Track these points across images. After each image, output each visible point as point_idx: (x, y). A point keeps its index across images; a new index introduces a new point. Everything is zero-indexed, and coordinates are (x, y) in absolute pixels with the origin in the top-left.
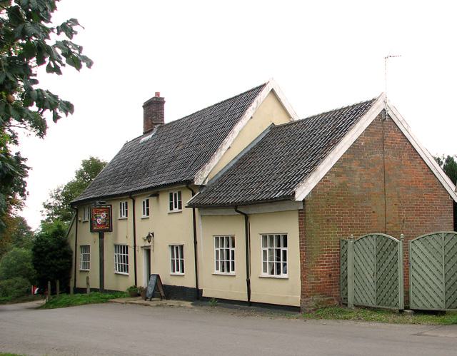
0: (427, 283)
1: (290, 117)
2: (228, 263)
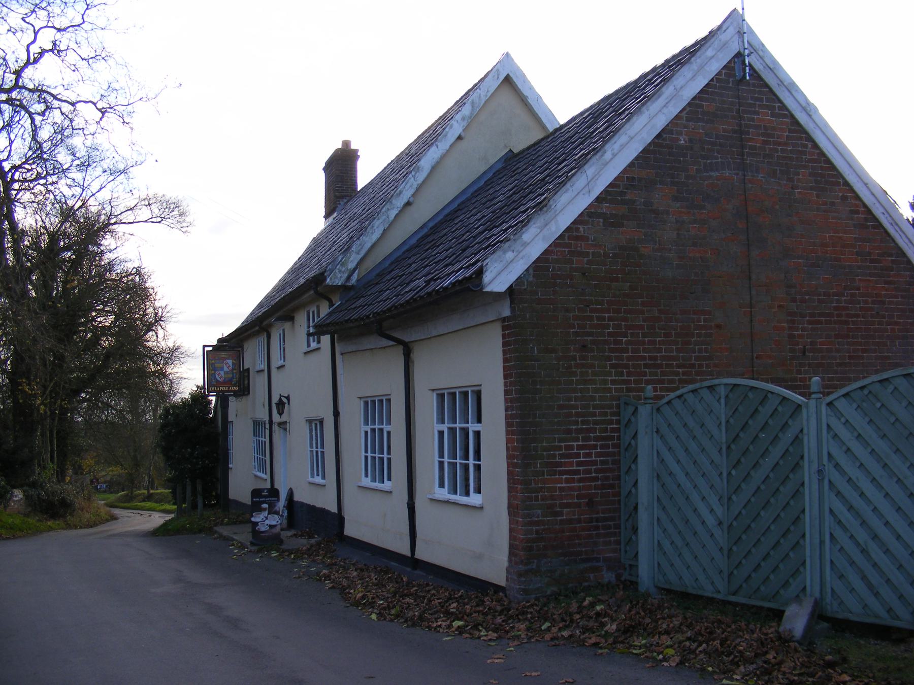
0: (875, 537)
1: (543, 126)
2: (466, 468)
